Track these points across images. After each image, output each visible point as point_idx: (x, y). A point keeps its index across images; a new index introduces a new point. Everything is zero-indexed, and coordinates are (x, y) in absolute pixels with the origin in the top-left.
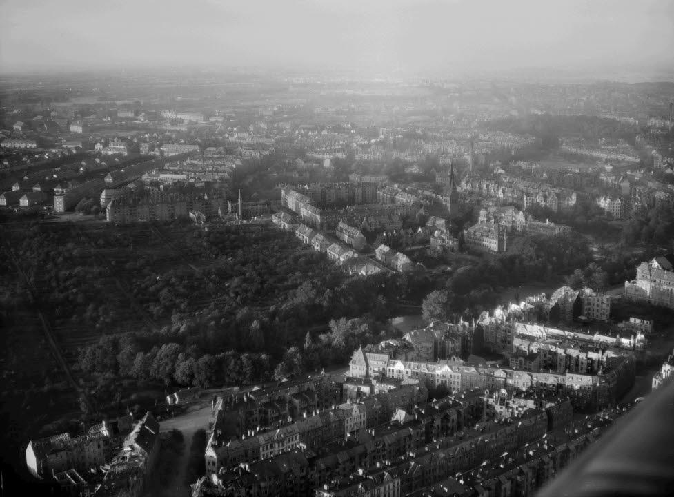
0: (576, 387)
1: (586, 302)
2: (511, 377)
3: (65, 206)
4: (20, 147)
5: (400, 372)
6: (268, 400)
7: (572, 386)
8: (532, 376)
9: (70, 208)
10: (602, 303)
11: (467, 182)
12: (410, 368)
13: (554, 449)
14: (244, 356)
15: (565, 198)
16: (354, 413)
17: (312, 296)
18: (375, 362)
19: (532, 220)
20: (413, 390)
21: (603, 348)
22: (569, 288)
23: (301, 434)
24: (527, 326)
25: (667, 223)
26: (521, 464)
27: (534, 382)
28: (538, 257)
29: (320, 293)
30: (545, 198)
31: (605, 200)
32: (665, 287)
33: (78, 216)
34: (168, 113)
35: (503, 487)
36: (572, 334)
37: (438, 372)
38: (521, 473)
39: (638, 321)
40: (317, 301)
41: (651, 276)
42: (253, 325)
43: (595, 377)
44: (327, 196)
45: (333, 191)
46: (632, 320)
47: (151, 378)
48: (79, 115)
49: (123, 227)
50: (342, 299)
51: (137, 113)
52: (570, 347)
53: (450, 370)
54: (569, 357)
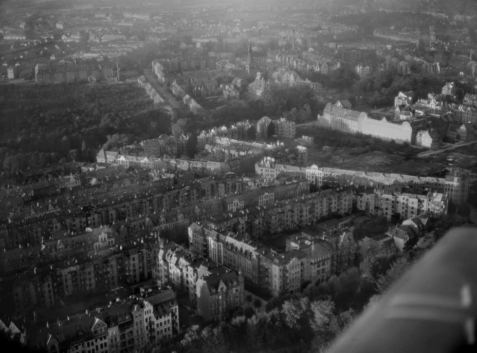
0: (212, 169)
1: (280, 126)
2: (179, 164)
3: (14, 74)
4: (15, 39)
5: (123, 161)
6: (31, 175)
7: (210, 168)
8: (189, 163)
9: (17, 76)
10: (290, 127)
11: (279, 56)
12: (128, 159)
13: (153, 196)
14: (40, 155)
15: (333, 65)
16: (71, 180)
17: (108, 122)
18: (110, 156)
19: (299, 79)
20: (115, 168)
21: (436, 165)
22: (267, 117)
23: (34, 190)
24: (222, 138)
25: (384, 81)
26: (126, 202)
27: (191, 166)
28: (275, 100)
29: (113, 120)
30: (320, 66)
31: (360, 67)
32: (338, 118)
33: (21, 81)
34: (127, 14)
35: (110, 213)
36: (242, 142)
37: (142, 161)
38: (124, 206)
39: (306, 137)
40: (111, 125)
41: (331, 111)
42: (63, 138)
43: (223, 163)
44: (182, 66)
45: (185, 63)
46: (303, 137)
47: (424, 214)
48: (68, 17)
49: (43, 86)
50: (127, 124)
51: (107, 15)
52: (232, 149)
53: (148, 160)
54: (231, 155)
